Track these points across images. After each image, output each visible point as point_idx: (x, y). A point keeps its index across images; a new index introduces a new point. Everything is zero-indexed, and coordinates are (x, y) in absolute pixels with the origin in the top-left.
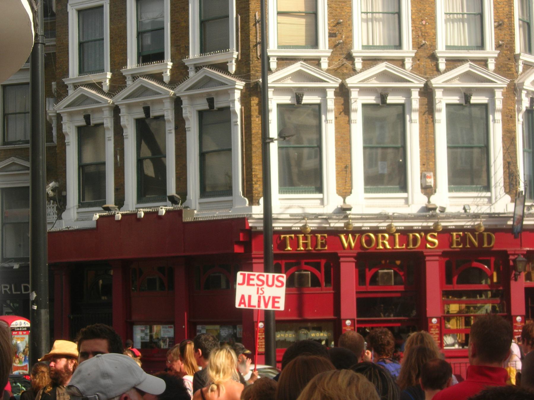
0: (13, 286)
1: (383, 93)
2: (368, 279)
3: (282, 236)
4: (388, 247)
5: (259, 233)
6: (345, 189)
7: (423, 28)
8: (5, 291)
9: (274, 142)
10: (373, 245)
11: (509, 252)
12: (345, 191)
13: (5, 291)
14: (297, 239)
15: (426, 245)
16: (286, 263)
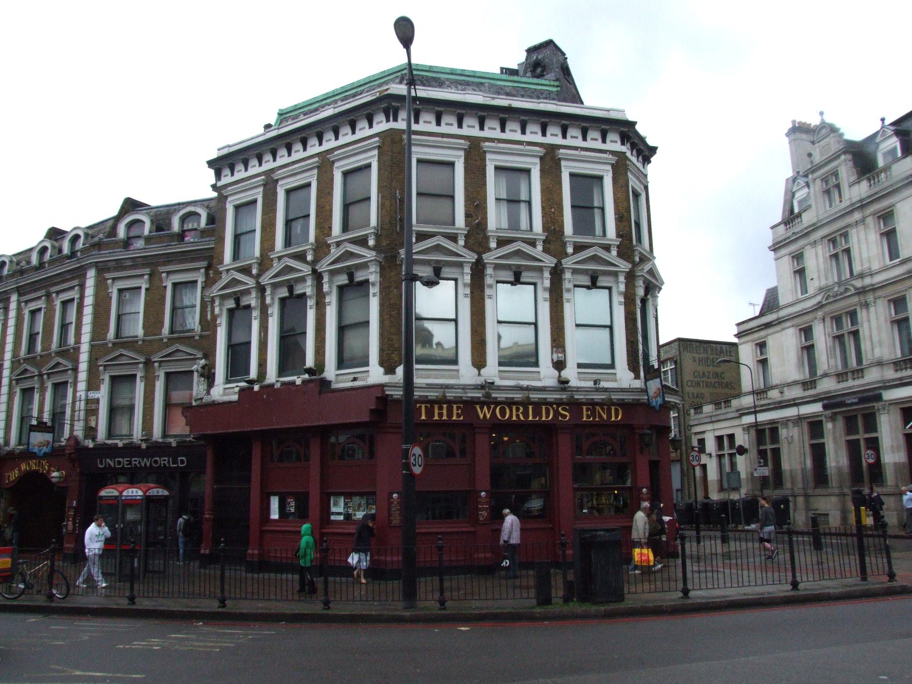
0: (171, 459)
4: (522, 418)
5: (397, 401)
8: (135, 464)
9: (518, 65)
10: (507, 416)
12: (480, 363)
13: (164, 464)
14: (433, 408)
15: (558, 418)
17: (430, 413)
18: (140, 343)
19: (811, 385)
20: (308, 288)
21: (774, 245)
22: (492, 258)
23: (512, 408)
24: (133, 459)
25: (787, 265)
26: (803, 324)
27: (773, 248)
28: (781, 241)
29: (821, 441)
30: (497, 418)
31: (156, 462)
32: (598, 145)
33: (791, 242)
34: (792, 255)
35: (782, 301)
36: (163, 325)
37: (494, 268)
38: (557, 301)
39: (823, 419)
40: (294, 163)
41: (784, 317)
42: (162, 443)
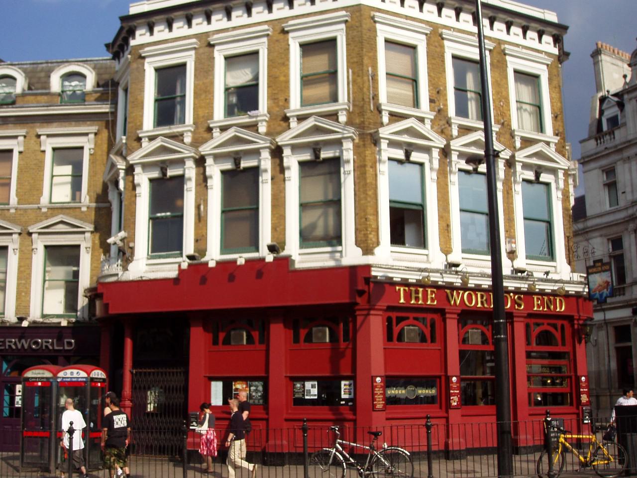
1: (236, 157)
2: (395, 335)
3: (397, 288)
6: (446, 247)
7: (501, 109)
8: (10, 346)
11: (446, 311)
12: (446, 249)
16: (397, 318)
17: (408, 296)
18: (12, 211)
19: (620, 292)
20: (266, 162)
21: (583, 158)
22: (208, 149)
23: (477, 294)
24: (7, 340)
25: (597, 178)
26: (613, 234)
27: (582, 161)
28: (592, 155)
29: (628, 344)
30: (465, 304)
31: (36, 343)
32: (535, 44)
33: (603, 156)
34: (603, 169)
35: (590, 211)
36: (41, 194)
37: (388, 144)
38: (508, 193)
39: (631, 324)
40: (234, 28)
41: (592, 227)
42: (42, 323)
